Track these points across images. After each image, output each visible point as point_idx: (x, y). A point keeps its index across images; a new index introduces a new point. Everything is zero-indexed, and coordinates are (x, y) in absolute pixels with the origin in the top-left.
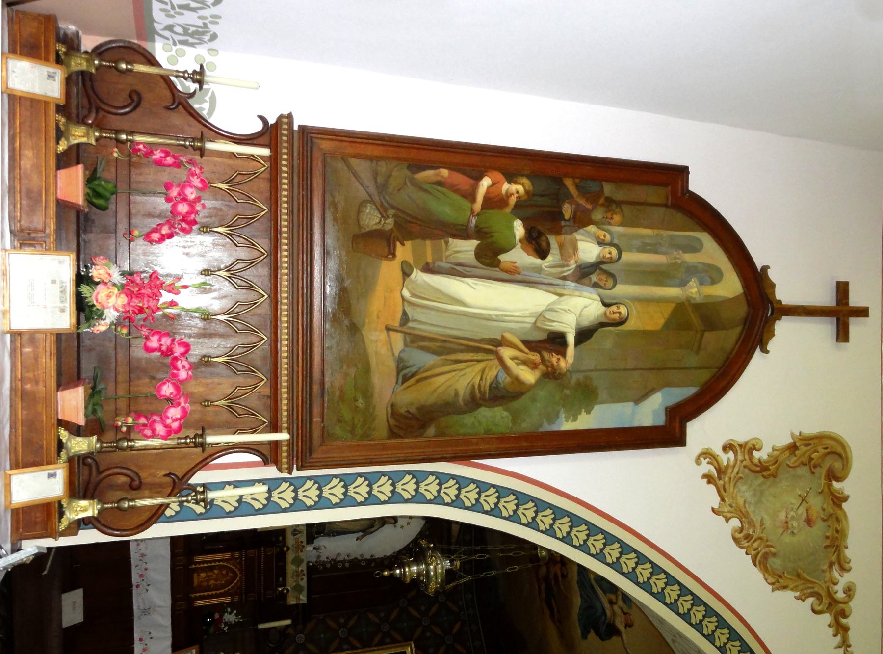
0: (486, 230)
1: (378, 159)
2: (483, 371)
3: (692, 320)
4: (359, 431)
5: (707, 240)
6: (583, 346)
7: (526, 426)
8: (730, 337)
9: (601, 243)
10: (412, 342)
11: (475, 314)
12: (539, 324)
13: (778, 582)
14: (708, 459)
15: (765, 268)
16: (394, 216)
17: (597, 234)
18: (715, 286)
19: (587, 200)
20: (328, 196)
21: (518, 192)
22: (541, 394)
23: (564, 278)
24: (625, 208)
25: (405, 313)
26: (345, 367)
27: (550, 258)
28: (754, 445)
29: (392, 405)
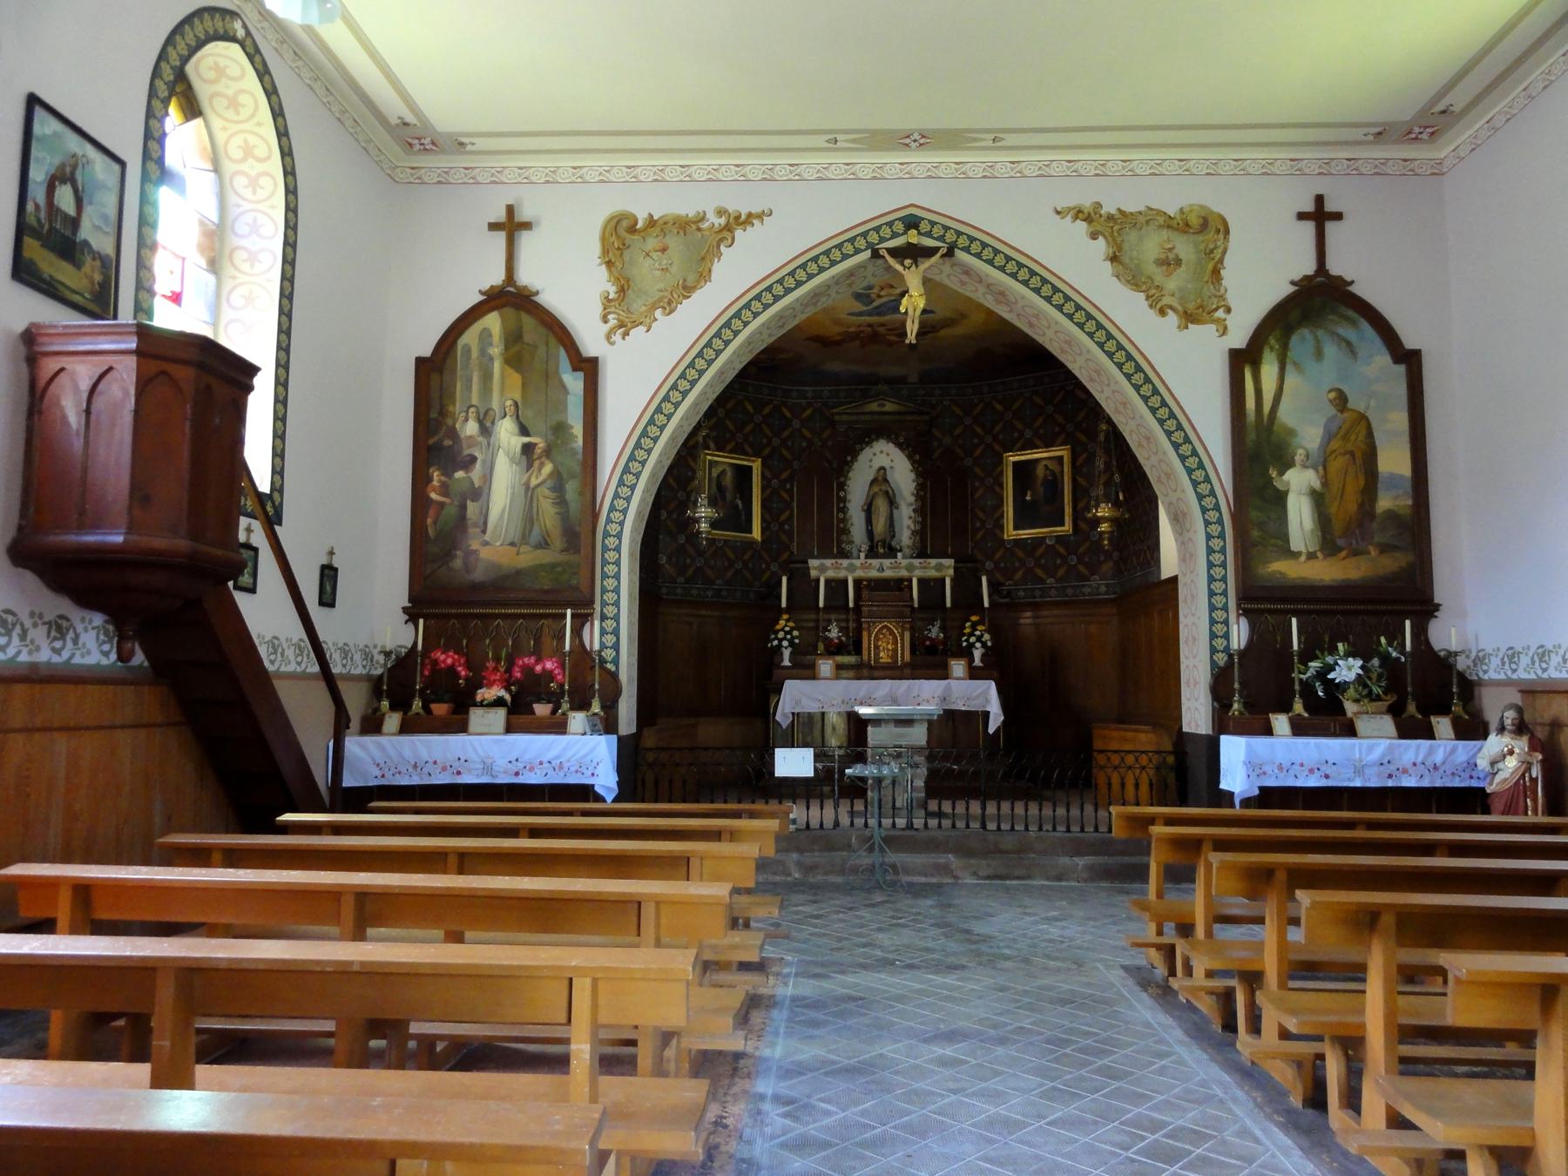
5: (462, 341)
7: (577, 469)
8: (528, 322)
9: (467, 420)
13: (704, 276)
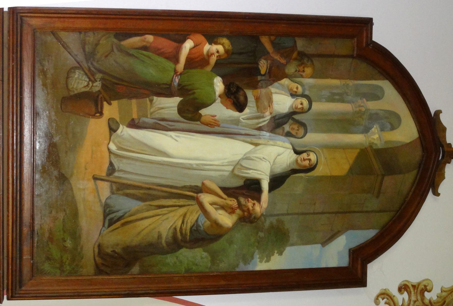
0: (189, 87)
1: (86, 30)
2: (185, 216)
3: (374, 164)
4: (67, 268)
6: (277, 191)
7: (223, 266)
8: (407, 181)
9: (293, 95)
10: (118, 189)
11: (178, 163)
12: (236, 172)
14: (385, 300)
15: (438, 113)
16: (102, 79)
17: (290, 87)
18: (395, 131)
19: (282, 55)
20: (38, 65)
21: (218, 52)
22: (238, 236)
23: (260, 129)
24: (317, 62)
25: (111, 164)
26: (54, 212)
27: (247, 110)
28: (425, 286)
29: (99, 246)
